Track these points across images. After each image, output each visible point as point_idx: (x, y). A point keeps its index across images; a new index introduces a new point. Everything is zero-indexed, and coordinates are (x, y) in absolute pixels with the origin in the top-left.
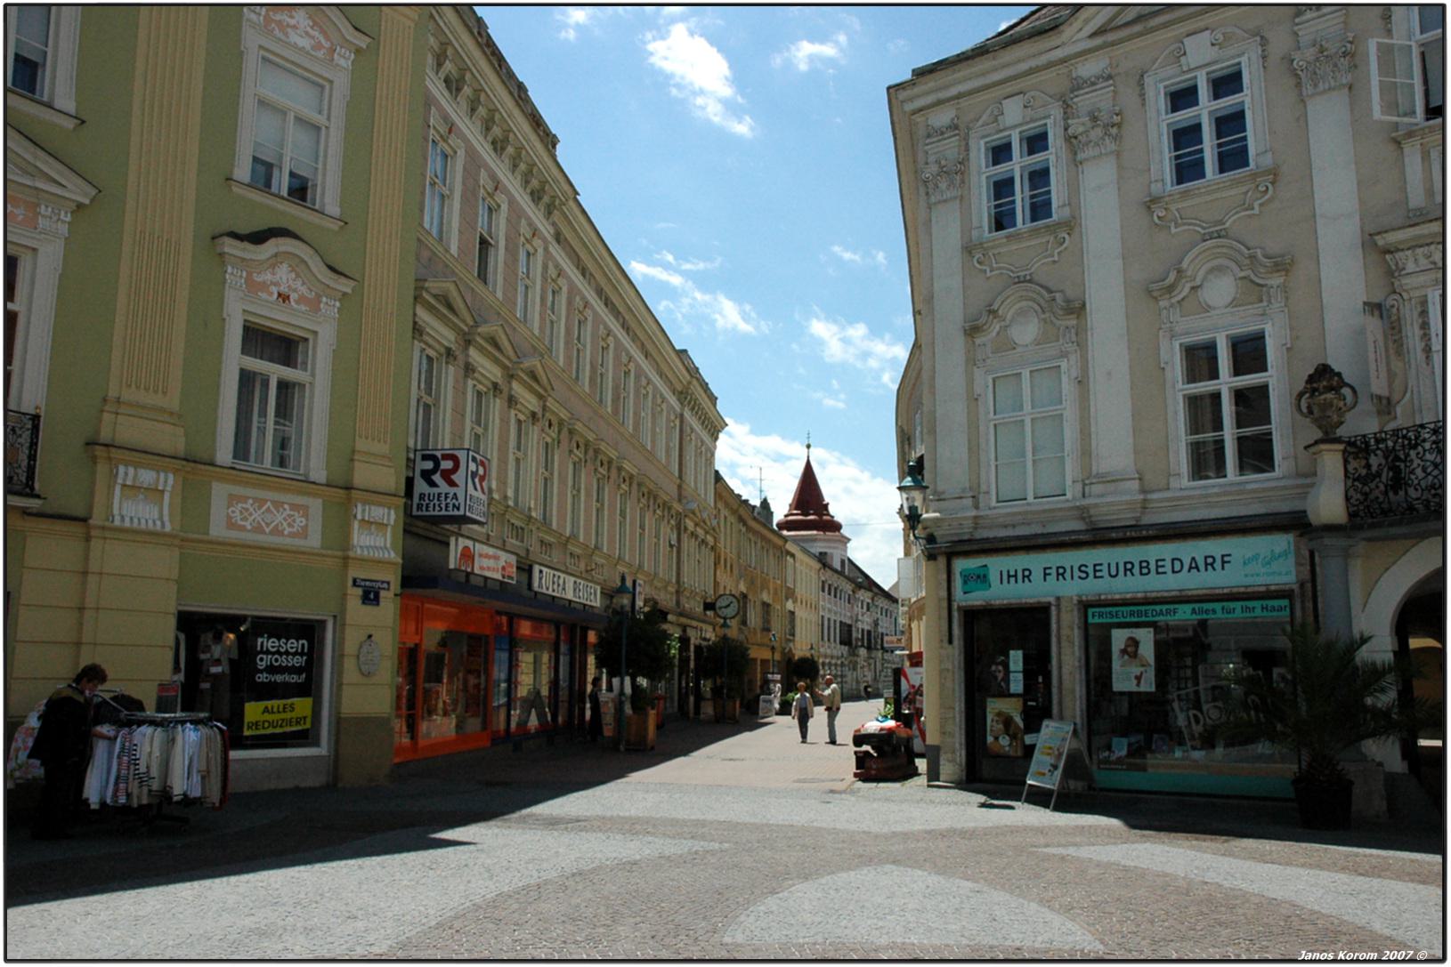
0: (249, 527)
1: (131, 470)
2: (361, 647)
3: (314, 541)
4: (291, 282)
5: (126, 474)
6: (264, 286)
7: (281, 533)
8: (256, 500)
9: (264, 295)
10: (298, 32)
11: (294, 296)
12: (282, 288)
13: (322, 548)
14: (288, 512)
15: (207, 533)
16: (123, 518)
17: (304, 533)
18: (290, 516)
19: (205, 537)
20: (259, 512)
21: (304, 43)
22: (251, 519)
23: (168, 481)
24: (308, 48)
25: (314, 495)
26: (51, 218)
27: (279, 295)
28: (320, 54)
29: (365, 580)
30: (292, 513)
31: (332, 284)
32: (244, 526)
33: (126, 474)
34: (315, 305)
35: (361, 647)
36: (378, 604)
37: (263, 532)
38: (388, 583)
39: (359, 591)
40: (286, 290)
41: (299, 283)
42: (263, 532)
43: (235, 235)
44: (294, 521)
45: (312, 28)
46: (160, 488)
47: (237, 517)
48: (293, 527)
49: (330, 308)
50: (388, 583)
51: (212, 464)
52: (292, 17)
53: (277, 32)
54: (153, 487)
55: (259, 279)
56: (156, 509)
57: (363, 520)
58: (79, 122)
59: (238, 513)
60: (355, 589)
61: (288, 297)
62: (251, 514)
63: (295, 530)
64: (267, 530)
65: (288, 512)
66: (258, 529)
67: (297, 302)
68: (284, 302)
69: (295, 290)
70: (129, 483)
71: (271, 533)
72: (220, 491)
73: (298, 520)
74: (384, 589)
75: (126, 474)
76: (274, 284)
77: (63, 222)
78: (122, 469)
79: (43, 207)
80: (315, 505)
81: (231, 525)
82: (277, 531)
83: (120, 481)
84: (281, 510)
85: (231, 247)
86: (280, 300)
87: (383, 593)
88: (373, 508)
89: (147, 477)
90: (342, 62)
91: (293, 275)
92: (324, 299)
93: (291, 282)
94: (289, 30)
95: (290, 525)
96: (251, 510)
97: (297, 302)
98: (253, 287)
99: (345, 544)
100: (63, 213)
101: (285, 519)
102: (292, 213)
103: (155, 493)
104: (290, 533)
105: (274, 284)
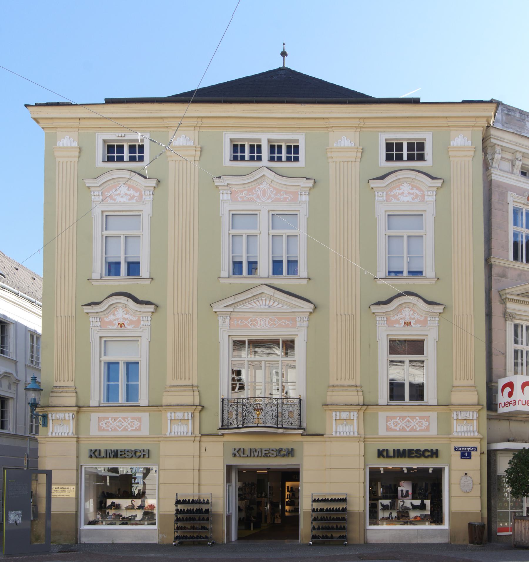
0: (398, 429)
1: (338, 413)
2: (461, 479)
3: (434, 431)
4: (411, 315)
5: (336, 415)
6: (111, 323)
7: (415, 430)
8: (400, 417)
9: (397, 326)
10: (404, 195)
11: (126, 323)
12: (406, 320)
13: (149, 435)
14: (418, 420)
15: (378, 435)
16: (336, 432)
17: (427, 429)
18: (419, 422)
19: (47, 437)
20: (403, 422)
21: (409, 198)
22: (399, 426)
23: (354, 415)
24: (411, 200)
25: (432, 411)
26: (301, 321)
27: (405, 323)
28: (418, 200)
29: (462, 448)
30: (133, 421)
31: (143, 310)
32: (396, 429)
33: (336, 415)
34: (424, 323)
35: (461, 479)
36: (470, 458)
37: (406, 431)
38: (476, 448)
39: (459, 453)
40: (409, 320)
41: (415, 315)
42: (406, 431)
43: (378, 303)
44: (422, 424)
45: (412, 189)
46: (352, 418)
47: (392, 426)
48: (422, 427)
49: (433, 322)
50: (476, 448)
51: (377, 405)
52: (400, 189)
53: (394, 200)
54: (348, 418)
55: (106, 320)
56: (296, 427)
57: (457, 419)
58: (437, 279)
59: (104, 424)
60: (456, 452)
61: (410, 323)
62: (399, 424)
63: (423, 428)
64: (408, 430)
65: (418, 420)
66: (403, 430)
67: (415, 324)
68: (408, 326)
69: (414, 318)
70: (338, 418)
71: (410, 431)
72: (382, 416)
73: (136, 424)
74: (473, 451)
75: (336, 415)
76: (401, 319)
77: (306, 321)
78: (334, 413)
79: (297, 318)
80: (433, 415)
81: (388, 429)
82: (413, 430)
83: (334, 418)
84: (415, 420)
85: (375, 309)
86: (406, 325)
87: (472, 453)
88: (462, 413)
89: (345, 415)
90: (430, 198)
91: (412, 312)
92: (429, 319)
93: (411, 315)
94: (400, 196)
95: (132, 426)
96: (399, 421)
97: (415, 324)
98: (390, 323)
99: (449, 431)
100: (304, 318)
101: (417, 424)
102: (412, 284)
103: (348, 421)
104: (420, 429)
105: (401, 319)
